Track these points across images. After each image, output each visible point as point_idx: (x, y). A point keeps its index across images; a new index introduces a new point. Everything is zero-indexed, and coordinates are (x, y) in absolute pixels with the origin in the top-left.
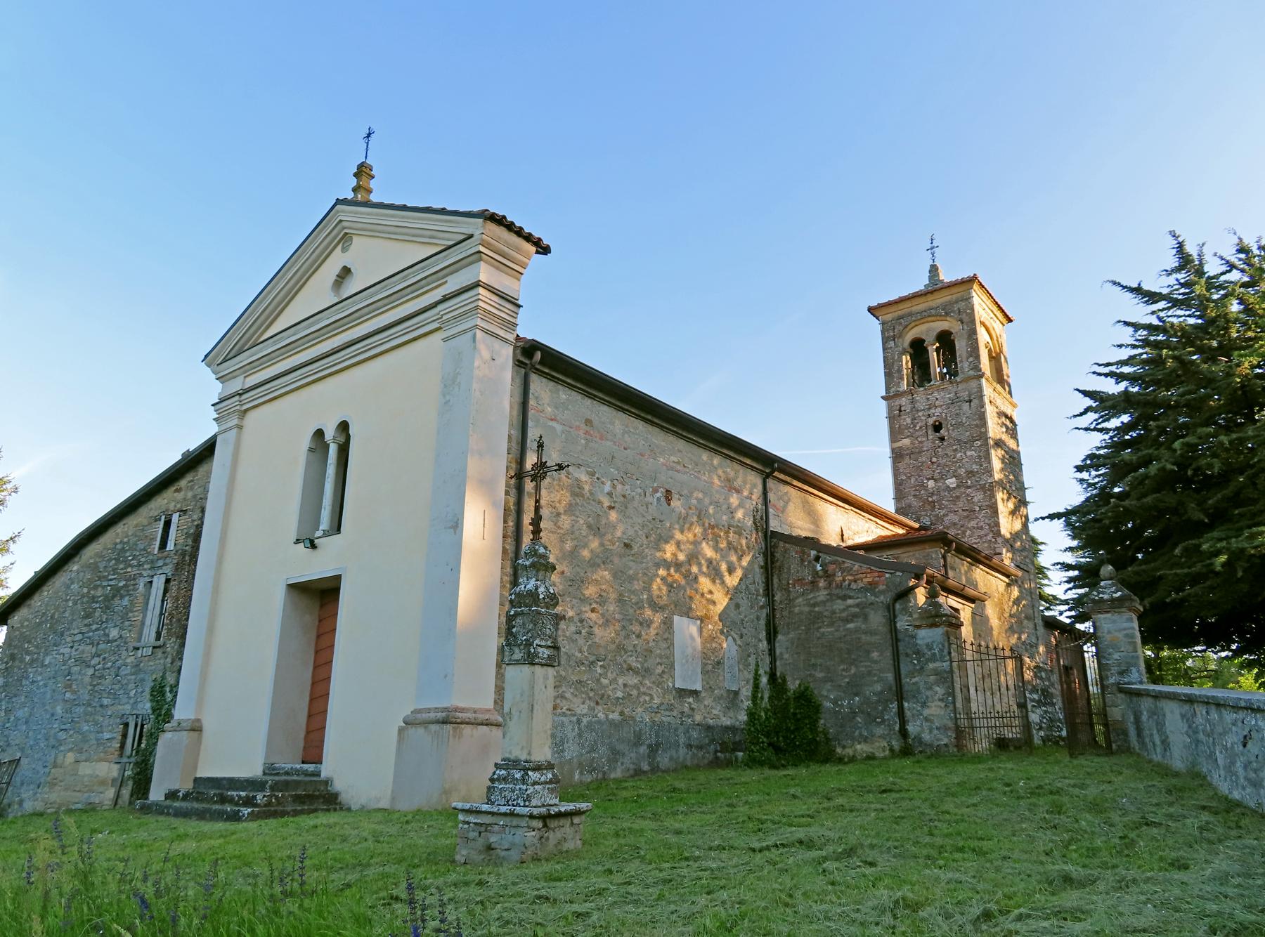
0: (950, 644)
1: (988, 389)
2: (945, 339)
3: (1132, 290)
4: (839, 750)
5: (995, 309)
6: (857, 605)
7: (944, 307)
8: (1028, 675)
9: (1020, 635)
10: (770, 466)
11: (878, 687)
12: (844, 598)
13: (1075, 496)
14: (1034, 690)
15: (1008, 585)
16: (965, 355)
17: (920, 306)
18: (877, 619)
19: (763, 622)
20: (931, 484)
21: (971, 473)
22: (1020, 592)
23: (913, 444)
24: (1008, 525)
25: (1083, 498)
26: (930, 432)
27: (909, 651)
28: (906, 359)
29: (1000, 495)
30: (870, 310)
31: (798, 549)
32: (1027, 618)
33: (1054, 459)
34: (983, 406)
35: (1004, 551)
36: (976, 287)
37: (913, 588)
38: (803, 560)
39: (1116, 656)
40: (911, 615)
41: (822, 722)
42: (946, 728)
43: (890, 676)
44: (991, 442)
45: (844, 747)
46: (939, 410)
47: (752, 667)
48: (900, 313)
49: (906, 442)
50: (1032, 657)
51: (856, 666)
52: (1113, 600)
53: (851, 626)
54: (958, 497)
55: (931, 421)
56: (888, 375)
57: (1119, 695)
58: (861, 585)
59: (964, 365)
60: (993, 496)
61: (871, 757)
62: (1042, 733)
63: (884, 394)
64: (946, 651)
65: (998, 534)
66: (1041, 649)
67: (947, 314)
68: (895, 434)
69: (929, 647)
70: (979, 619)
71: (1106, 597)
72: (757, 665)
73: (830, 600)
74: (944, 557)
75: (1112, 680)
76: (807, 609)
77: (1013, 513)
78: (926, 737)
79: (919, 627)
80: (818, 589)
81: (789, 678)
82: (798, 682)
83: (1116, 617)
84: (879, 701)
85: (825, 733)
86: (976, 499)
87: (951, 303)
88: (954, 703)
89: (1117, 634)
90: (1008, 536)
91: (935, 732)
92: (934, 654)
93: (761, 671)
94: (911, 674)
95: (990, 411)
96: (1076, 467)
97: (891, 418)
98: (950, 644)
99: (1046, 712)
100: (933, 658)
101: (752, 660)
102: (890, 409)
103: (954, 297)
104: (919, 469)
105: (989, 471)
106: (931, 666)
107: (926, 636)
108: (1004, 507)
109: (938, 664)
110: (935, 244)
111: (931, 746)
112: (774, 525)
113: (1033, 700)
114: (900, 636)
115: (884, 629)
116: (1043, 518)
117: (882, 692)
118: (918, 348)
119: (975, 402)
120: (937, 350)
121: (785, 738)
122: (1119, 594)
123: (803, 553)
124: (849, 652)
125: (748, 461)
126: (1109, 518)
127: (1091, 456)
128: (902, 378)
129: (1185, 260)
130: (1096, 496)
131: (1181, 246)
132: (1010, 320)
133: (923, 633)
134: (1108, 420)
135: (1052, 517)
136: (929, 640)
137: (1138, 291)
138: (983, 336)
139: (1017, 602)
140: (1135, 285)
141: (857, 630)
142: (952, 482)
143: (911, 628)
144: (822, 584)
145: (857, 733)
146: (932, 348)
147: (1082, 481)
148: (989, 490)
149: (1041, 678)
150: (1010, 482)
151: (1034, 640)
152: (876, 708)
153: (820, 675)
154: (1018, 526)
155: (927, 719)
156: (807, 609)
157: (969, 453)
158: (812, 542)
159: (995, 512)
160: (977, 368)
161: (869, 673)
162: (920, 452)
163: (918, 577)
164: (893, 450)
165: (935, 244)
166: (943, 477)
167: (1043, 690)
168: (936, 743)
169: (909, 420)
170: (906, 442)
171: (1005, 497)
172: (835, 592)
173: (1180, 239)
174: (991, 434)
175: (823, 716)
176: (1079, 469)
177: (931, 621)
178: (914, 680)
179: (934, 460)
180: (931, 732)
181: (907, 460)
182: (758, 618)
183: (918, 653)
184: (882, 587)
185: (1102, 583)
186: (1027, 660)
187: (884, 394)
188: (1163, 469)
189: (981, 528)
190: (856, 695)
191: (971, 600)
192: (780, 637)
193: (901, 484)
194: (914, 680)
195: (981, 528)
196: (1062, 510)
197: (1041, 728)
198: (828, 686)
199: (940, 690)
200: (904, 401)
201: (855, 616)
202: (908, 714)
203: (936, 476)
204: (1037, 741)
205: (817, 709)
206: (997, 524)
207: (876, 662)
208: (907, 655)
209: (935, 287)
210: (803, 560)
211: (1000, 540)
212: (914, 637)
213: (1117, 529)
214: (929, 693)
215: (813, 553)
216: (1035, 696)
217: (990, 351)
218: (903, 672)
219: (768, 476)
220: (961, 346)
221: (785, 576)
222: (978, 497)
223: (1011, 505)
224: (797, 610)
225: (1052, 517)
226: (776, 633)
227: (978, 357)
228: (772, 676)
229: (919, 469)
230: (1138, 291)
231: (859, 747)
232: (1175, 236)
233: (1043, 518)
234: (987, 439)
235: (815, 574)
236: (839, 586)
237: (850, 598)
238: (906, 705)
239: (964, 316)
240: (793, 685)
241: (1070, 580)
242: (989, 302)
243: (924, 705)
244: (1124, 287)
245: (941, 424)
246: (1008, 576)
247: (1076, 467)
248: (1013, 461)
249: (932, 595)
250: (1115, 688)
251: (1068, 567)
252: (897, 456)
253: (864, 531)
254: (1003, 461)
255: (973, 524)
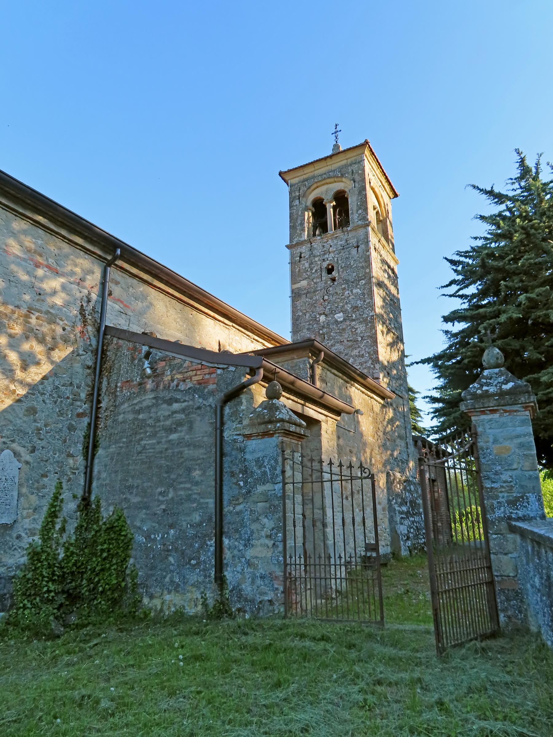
0: (284, 459)
1: (374, 239)
2: (341, 199)
3: (486, 192)
4: (146, 601)
5: (384, 181)
6: (183, 410)
7: (341, 169)
8: (398, 488)
9: (393, 451)
10: (111, 251)
11: (196, 517)
12: (170, 402)
13: (440, 344)
14: (403, 502)
15: (383, 406)
16: (355, 209)
17: (322, 169)
18: (203, 427)
19: (80, 434)
20: (322, 318)
21: (355, 308)
22: (395, 414)
23: (309, 284)
24: (385, 354)
25: (446, 346)
26: (324, 273)
27: (236, 469)
28: (308, 215)
29: (380, 327)
30: (281, 174)
31: (131, 345)
32: (400, 437)
33: (427, 323)
34: (368, 250)
35: (381, 376)
36: (367, 152)
37: (245, 386)
38: (133, 359)
39: (505, 477)
40: (240, 422)
41: (132, 561)
42: (272, 577)
43: (211, 502)
44: (374, 280)
45: (152, 597)
46: (332, 255)
47: (51, 490)
48: (305, 177)
49: (304, 283)
50: (402, 472)
51: (175, 490)
52: (502, 394)
53: (174, 436)
54: (344, 330)
55: (325, 265)
56: (293, 228)
57: (510, 536)
58: (190, 385)
59: (354, 216)
60: (374, 327)
61: (179, 617)
62: (409, 543)
63: (288, 243)
64: (279, 469)
65: (377, 360)
66: (411, 464)
67: (342, 175)
68: (294, 278)
69: (259, 463)
70: (348, 434)
71: (492, 389)
72: (60, 486)
73: (156, 405)
74: (312, 367)
75: (499, 513)
76: (131, 417)
77: (392, 345)
78: (247, 588)
79: (248, 437)
80: (145, 391)
81: (103, 503)
82: (111, 508)
83: (506, 418)
84: (196, 536)
85: (134, 577)
86: (359, 331)
87: (346, 166)
88: (284, 541)
89: (507, 444)
90: (386, 363)
91: (259, 582)
92: (265, 473)
93: (66, 495)
94: (235, 500)
95: (374, 255)
96: (444, 317)
97: (293, 263)
98: (284, 459)
99: (413, 522)
100: (263, 480)
101: (50, 482)
102: (292, 256)
103: (349, 161)
104: (313, 305)
105: (372, 306)
106: (261, 489)
107: (257, 448)
108: (383, 340)
109: (268, 487)
110: (338, 129)
111: (253, 601)
112: (111, 320)
113: (401, 513)
114: (227, 449)
115: (209, 440)
116: (417, 363)
117: (200, 524)
118: (319, 208)
119: (362, 247)
120: (334, 208)
121: (90, 580)
122: (510, 385)
123: (135, 349)
124: (169, 470)
125: (79, 241)
126: (469, 357)
127: (454, 312)
128: (303, 230)
129: (525, 171)
130: (456, 343)
131: (522, 160)
132: (396, 195)
133: (252, 444)
134: (467, 286)
135: (423, 362)
136: (260, 454)
137: (490, 193)
138: (372, 200)
139: (391, 421)
140: (489, 189)
141: (180, 442)
142: (339, 316)
143: (240, 438)
144: (149, 385)
145: (167, 579)
146: (329, 208)
147: (447, 332)
148: (370, 323)
149: (410, 491)
150: (390, 319)
151: (405, 457)
152: (192, 545)
153: (135, 500)
154: (395, 357)
155: (249, 564)
156: (131, 417)
157: (355, 291)
158: (147, 337)
159: (375, 342)
160: (364, 218)
161: (189, 498)
162: (315, 291)
163: (253, 372)
164: (293, 291)
165: (338, 129)
166: (333, 312)
167: (411, 502)
168: (258, 598)
169: (307, 265)
170: (304, 283)
171: (385, 331)
172: (161, 395)
173: (522, 156)
174: (374, 274)
175: (132, 553)
176: (446, 319)
177: (262, 428)
178: (238, 508)
179: (326, 297)
180: (253, 582)
181: (303, 298)
182: (71, 428)
183: (245, 471)
184: (211, 387)
185: (486, 373)
186: (398, 475)
187: (288, 243)
188: (510, 318)
189: (363, 356)
190: (171, 526)
191: (337, 412)
192: (100, 452)
193: (297, 320)
194: (238, 508)
195: (363, 356)
196: (431, 356)
197: (408, 538)
198: (142, 514)
199: (268, 523)
200: (304, 249)
201: (179, 424)
202: (227, 555)
203: (327, 311)
204: (404, 553)
205: (127, 544)
206: (376, 352)
207: (197, 484)
208: (233, 474)
209: (337, 153)
210: (133, 359)
211: (377, 366)
212: (242, 450)
213: (471, 372)
214: (254, 527)
215: (145, 349)
216: (404, 509)
217: (377, 213)
218: (226, 497)
219: (109, 264)
220: (353, 202)
221: (114, 377)
222: (361, 328)
223: (389, 338)
224: (121, 418)
225: (423, 362)
226: (95, 446)
227: (366, 209)
228: (86, 501)
229: (313, 305)
230: (490, 193)
231: (167, 597)
232: (519, 153)
233: (417, 363)
234: (370, 278)
235: (144, 376)
236: (167, 388)
237: (177, 401)
238: (226, 541)
239: (357, 177)
240: (107, 513)
241: (436, 411)
242: (378, 171)
243: (248, 544)
244: (481, 190)
245: (333, 267)
246: (383, 398)
247: (444, 317)
248: (393, 304)
249: (272, 395)
250: (504, 525)
251: (434, 400)
252: (296, 295)
253: (242, 343)
254: (384, 299)
255: (356, 352)
